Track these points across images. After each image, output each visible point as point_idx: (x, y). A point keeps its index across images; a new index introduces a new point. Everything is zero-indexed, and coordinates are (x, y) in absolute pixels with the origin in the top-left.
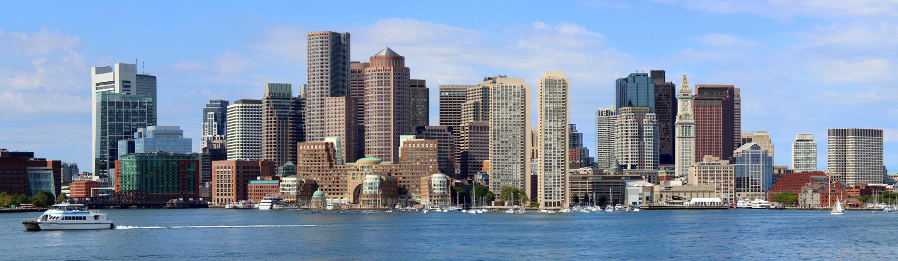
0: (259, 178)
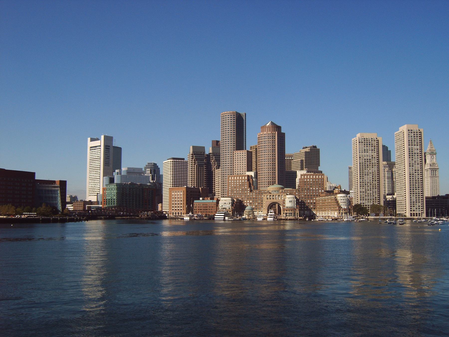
0: (201, 199)
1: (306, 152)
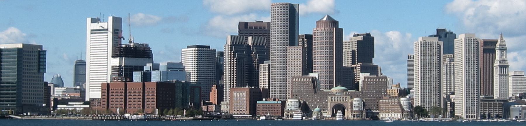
0: (264, 99)
1: (358, 41)
